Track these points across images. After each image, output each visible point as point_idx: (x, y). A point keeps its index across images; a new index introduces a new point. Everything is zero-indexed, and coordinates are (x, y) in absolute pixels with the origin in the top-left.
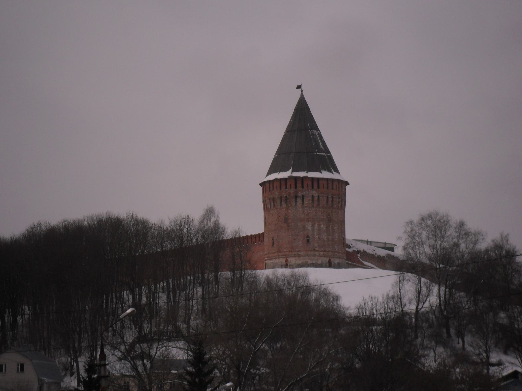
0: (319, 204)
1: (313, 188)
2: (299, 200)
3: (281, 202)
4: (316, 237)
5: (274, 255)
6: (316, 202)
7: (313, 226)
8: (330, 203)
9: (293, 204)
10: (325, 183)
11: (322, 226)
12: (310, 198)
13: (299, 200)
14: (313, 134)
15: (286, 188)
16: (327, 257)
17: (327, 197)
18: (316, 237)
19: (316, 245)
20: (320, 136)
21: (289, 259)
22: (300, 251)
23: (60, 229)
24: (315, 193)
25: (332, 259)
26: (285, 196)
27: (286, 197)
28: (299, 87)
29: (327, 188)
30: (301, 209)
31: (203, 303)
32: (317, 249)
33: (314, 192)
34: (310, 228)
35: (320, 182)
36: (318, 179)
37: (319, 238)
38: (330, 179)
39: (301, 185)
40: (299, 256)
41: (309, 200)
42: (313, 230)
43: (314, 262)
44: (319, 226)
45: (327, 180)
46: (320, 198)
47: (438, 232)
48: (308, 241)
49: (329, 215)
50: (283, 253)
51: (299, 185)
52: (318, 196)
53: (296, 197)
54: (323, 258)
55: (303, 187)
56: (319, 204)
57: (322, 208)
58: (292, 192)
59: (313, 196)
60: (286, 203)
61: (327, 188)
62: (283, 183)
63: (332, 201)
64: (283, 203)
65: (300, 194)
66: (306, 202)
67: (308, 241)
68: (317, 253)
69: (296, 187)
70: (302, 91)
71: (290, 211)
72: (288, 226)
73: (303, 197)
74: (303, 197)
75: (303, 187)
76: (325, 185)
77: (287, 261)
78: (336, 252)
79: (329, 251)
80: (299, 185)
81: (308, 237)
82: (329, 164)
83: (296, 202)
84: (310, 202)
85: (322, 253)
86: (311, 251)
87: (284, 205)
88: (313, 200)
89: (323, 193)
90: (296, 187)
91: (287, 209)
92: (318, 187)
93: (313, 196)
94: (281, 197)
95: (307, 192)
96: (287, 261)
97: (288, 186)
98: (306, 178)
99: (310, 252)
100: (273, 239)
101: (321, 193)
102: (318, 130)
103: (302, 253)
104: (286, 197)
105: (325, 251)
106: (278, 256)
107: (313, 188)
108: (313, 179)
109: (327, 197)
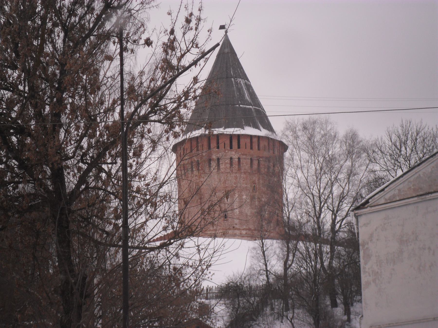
0: (239, 169)
1: (231, 148)
2: (214, 164)
3: (192, 168)
6: (235, 166)
9: (207, 170)
10: (248, 140)
11: (244, 197)
12: (228, 161)
14: (237, 83)
20: (249, 87)
24: (235, 155)
27: (198, 161)
28: (222, 27)
29: (251, 148)
32: (237, 226)
33: (233, 153)
35: (242, 141)
36: (239, 136)
37: (241, 212)
38: (255, 136)
44: (240, 196)
45: (251, 137)
47: (403, 149)
51: (213, 144)
52: (239, 159)
53: (210, 160)
56: (239, 169)
57: (245, 173)
59: (231, 158)
60: (198, 170)
61: (251, 148)
62: (194, 143)
65: (214, 157)
66: (222, 166)
68: (237, 232)
70: (226, 32)
73: (218, 159)
74: (218, 159)
75: (218, 147)
76: (248, 145)
80: (213, 144)
82: (261, 119)
84: (228, 166)
85: (244, 232)
87: (196, 172)
88: (231, 164)
89: (246, 155)
92: (239, 147)
93: (231, 158)
98: (222, 134)
101: (243, 155)
102: (245, 77)
104: (198, 161)
107: (231, 148)
108: (231, 137)
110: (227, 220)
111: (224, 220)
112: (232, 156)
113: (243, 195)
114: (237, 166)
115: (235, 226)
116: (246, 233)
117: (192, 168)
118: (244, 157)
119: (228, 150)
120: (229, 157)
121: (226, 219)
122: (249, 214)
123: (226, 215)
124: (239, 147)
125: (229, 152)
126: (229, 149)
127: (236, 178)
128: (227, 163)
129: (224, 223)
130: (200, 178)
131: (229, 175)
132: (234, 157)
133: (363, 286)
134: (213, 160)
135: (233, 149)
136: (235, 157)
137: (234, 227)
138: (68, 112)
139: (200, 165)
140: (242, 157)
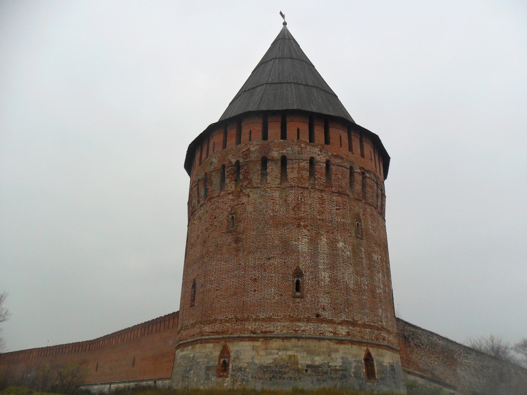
1: (311, 139)
2: (274, 169)
3: (223, 180)
4: (325, 275)
5: (192, 331)
7: (313, 242)
8: (358, 187)
9: (256, 178)
11: (341, 244)
13: (274, 169)
15: (239, 142)
16: (360, 343)
17: (352, 174)
18: (325, 275)
19: (324, 301)
21: (234, 348)
22: (270, 320)
23: (487, 350)
25: (373, 352)
26: (234, 161)
27: (238, 162)
30: (277, 194)
31: (202, 342)
32: (326, 315)
33: (317, 150)
34: (303, 246)
37: (334, 280)
39: (279, 131)
40: (267, 337)
41: (300, 169)
42: (314, 254)
43: (318, 360)
44: (332, 243)
46: (333, 168)
48: (298, 287)
49: (357, 217)
50: (217, 327)
52: (328, 163)
53: (264, 162)
54: (348, 346)
55: (284, 136)
58: (252, 149)
59: (312, 161)
63: (364, 185)
64: (227, 181)
66: (292, 175)
67: (298, 287)
69: (265, 137)
71: (244, 200)
72: (237, 241)
73: (284, 161)
74: (284, 161)
75: (284, 136)
77: (225, 352)
78: (383, 329)
79: (365, 326)
81: (298, 273)
83: (264, 174)
84: (306, 174)
85: (343, 330)
86: (309, 320)
87: (231, 186)
90: (265, 137)
91: (238, 194)
92: (327, 142)
93: (312, 161)
94: (224, 166)
95: (296, 148)
96: (225, 352)
97: (245, 137)
99: (302, 326)
100: (194, 286)
101: (336, 156)
103: (278, 328)
105: (354, 324)
106: (202, 333)
107: (311, 139)
109: (352, 174)
110: (301, 297)
111: (295, 297)
112: (314, 155)
113: (337, 241)
114: (324, 178)
115: (320, 312)
116: (348, 334)
117: (223, 180)
118: (338, 161)
119: (306, 144)
120: (306, 156)
121: (298, 294)
122: (352, 286)
123: (298, 283)
124: (327, 142)
125: (308, 147)
126: (308, 141)
127: (322, 201)
128: (303, 169)
129: (294, 302)
130: (239, 197)
131: (306, 193)
132: (318, 158)
133: (337, 115)
134: (273, 160)
135: (316, 142)
136: (321, 158)
137: (318, 316)
138: (363, 256)
139: (242, 171)
140: (333, 160)
